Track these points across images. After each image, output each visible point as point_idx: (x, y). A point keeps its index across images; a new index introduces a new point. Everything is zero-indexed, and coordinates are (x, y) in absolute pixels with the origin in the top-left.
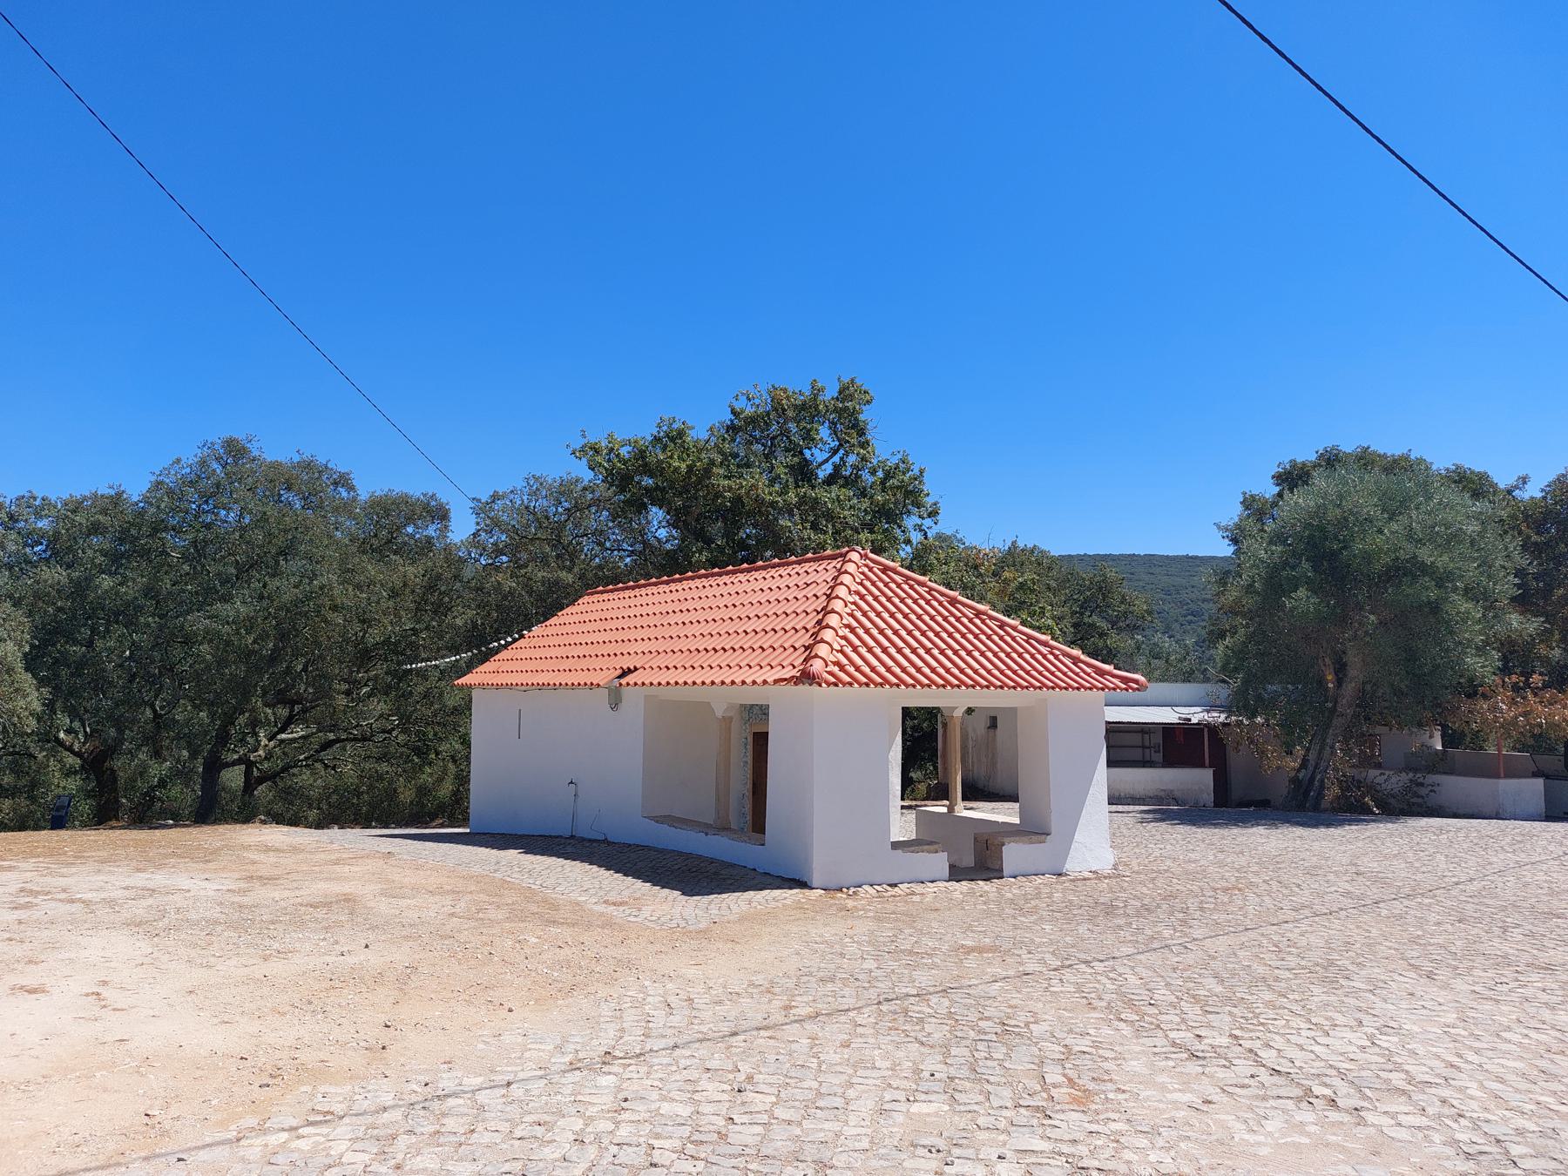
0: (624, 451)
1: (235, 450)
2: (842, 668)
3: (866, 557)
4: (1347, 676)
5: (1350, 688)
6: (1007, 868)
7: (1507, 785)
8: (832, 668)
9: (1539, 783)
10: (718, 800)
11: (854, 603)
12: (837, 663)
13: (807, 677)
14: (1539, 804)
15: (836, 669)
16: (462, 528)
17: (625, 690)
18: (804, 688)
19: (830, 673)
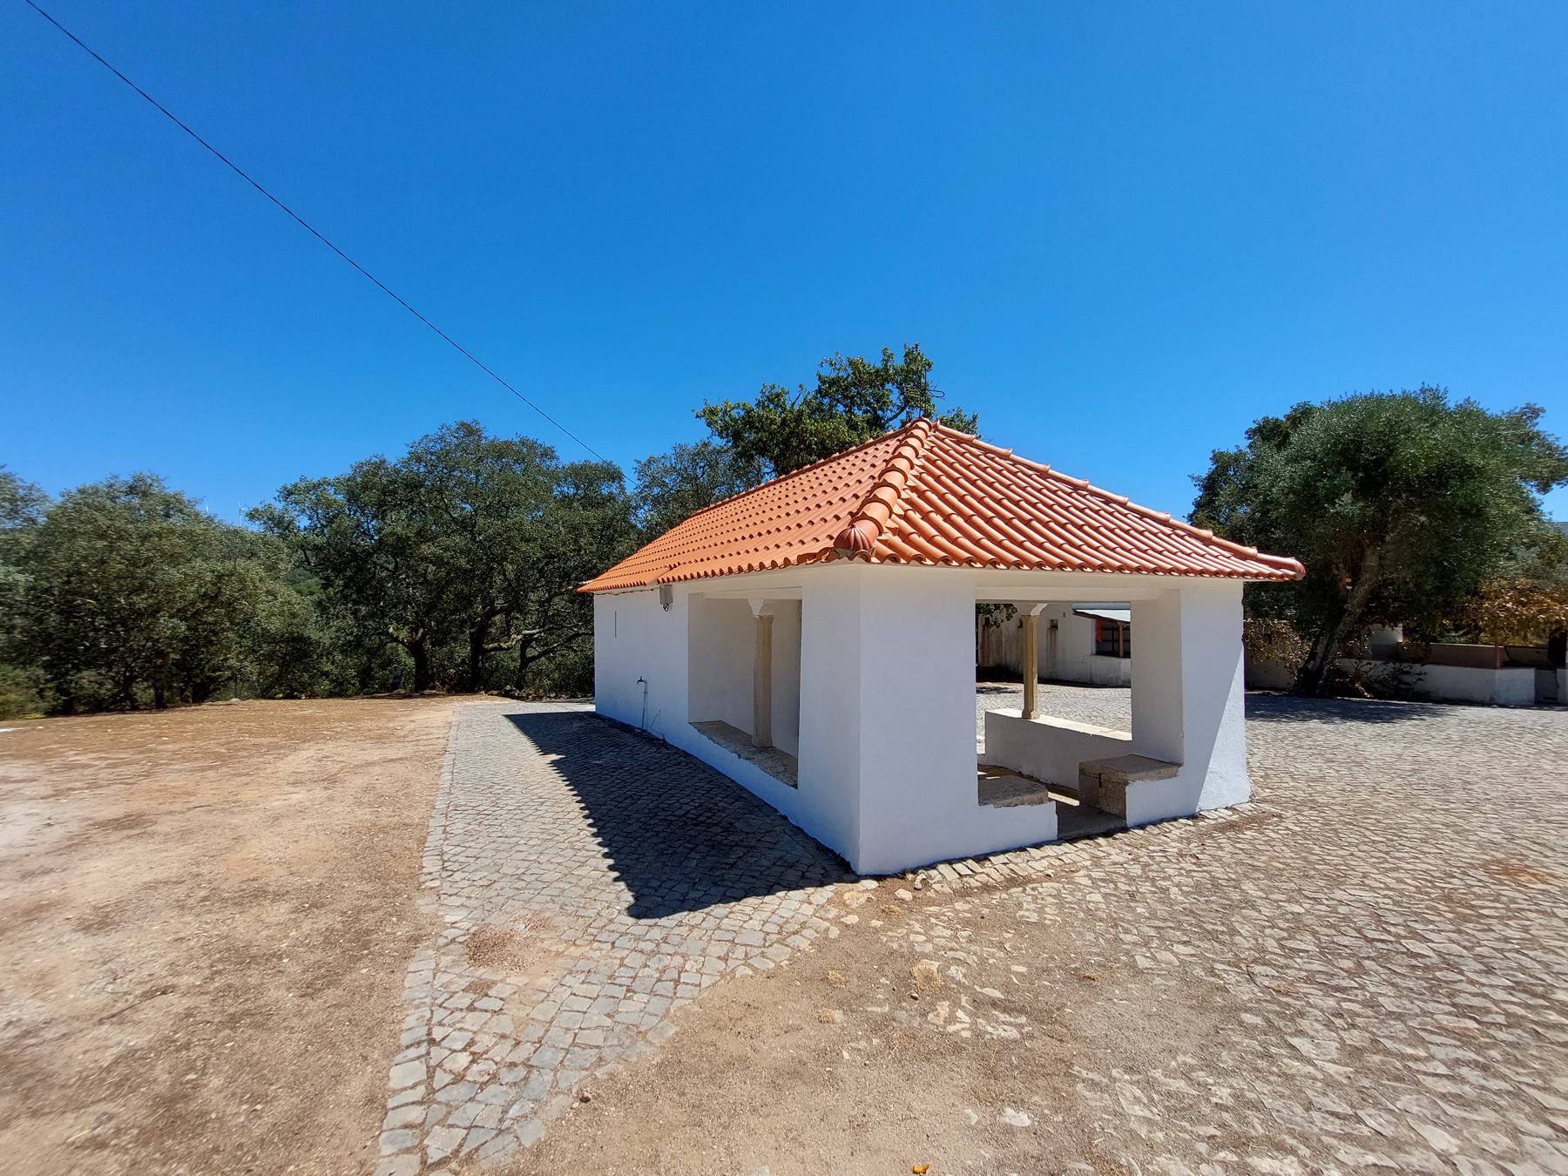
0: (734, 413)
1: (469, 430)
2: (906, 538)
3: (936, 428)
4: (1375, 573)
5: (1363, 590)
6: (1130, 821)
7: (1503, 675)
8: (888, 536)
9: (1529, 674)
10: (756, 714)
11: (923, 467)
12: (897, 532)
13: (846, 547)
14: (1529, 692)
15: (897, 540)
16: (631, 485)
17: (676, 586)
18: (845, 569)
19: (885, 542)
